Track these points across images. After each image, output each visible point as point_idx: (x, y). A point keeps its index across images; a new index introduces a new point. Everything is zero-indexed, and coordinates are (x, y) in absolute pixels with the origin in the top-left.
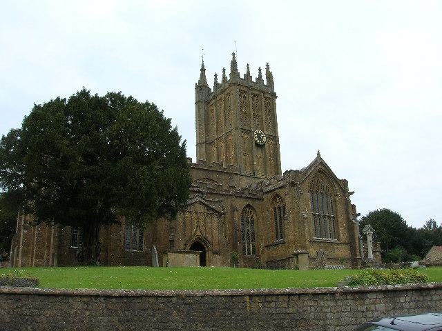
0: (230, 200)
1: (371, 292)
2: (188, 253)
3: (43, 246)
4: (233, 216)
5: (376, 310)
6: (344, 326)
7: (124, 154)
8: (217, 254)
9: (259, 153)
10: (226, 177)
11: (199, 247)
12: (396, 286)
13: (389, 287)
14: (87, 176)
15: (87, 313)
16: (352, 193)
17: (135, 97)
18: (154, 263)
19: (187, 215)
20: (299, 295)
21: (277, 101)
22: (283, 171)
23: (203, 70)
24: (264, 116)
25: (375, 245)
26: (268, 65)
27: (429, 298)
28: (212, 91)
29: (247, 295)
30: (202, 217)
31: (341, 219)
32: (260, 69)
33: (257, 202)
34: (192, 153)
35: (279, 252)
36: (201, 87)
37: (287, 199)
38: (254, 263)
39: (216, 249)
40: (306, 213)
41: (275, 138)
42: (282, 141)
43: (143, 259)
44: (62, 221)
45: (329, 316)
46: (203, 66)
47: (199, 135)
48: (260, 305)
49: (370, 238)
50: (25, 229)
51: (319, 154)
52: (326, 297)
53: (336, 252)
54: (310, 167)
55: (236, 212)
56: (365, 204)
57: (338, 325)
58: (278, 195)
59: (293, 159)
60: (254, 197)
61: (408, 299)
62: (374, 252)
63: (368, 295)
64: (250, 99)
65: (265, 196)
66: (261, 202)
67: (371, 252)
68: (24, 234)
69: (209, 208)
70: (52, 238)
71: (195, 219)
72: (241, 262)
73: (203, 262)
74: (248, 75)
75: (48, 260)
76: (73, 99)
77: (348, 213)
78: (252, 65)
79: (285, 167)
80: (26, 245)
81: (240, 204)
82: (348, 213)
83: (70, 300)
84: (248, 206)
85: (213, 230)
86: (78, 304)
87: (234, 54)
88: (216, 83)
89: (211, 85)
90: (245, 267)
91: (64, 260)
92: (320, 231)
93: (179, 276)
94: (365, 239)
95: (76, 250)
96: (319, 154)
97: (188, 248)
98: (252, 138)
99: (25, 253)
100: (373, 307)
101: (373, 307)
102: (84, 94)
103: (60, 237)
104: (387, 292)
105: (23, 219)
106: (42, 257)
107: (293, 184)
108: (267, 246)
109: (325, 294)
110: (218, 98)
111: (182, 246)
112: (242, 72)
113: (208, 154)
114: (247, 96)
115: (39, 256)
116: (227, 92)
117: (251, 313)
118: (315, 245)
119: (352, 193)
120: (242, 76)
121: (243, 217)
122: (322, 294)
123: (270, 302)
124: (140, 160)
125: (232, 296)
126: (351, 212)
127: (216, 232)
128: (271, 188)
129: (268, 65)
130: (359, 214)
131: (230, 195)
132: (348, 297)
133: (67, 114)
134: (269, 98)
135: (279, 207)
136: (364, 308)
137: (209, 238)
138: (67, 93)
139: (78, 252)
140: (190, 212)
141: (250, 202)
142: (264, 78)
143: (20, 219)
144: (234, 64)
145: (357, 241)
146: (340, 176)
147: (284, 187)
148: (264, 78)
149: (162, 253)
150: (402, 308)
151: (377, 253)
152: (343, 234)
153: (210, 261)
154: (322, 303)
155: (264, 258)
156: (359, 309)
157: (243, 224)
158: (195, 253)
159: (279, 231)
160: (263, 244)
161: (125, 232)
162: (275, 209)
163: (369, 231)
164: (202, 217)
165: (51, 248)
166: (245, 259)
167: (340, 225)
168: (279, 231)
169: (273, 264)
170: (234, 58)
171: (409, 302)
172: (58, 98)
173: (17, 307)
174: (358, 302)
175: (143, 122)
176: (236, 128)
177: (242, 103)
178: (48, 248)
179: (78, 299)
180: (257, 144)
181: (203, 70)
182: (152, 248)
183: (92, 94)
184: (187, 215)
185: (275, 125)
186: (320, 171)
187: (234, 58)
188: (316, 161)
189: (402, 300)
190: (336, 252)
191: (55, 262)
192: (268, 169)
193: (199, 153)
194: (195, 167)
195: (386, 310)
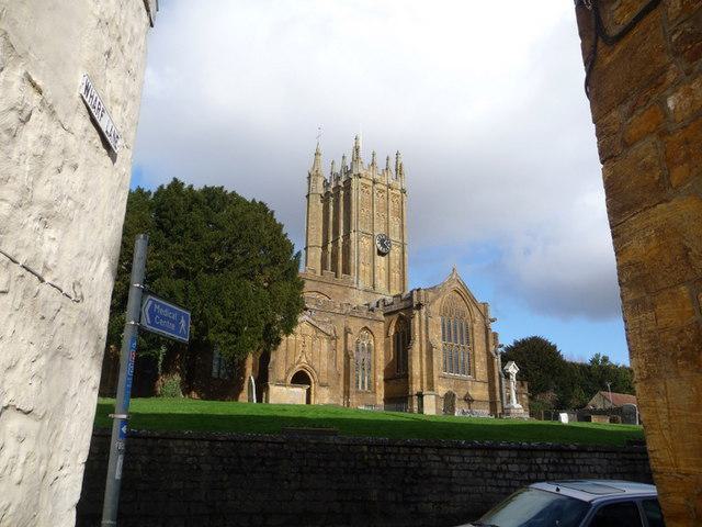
4: (346, 341)
7: (31, 203)
30: (309, 339)
36: (130, 192)
39: (324, 380)
45: (454, 473)
49: (513, 378)
61: (546, 461)
63: (500, 453)
97: (289, 382)
100: (504, 467)
101: (504, 467)
121: (357, 342)
127: (325, 360)
136: (494, 468)
150: (539, 471)
151: (524, 396)
157: (357, 350)
167: (477, 358)
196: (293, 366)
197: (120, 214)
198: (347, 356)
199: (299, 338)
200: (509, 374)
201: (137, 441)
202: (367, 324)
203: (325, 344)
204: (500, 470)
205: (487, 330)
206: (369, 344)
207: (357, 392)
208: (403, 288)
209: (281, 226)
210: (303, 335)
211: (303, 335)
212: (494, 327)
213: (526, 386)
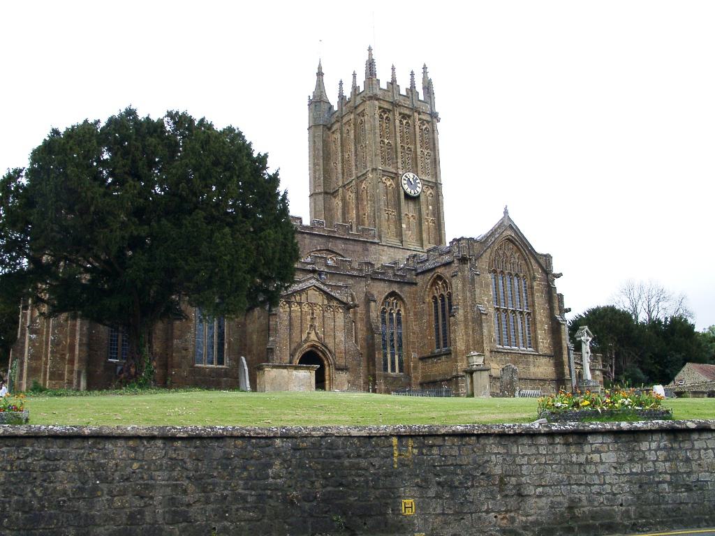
0: (363, 284)
1: (595, 432)
2: (296, 368)
3: (63, 357)
4: (368, 311)
5: (602, 463)
6: (550, 486)
8: (342, 370)
9: (408, 210)
10: (359, 248)
11: (312, 358)
12: (635, 424)
13: (624, 425)
14: (136, 243)
15: (135, 466)
16: (559, 276)
17: (209, 120)
18: (242, 387)
19: (295, 308)
20: (478, 436)
21: (439, 126)
22: (449, 237)
23: (320, 74)
24: (419, 150)
25: (594, 358)
26: (425, 68)
27: (687, 445)
28: (336, 108)
29: (393, 436)
30: (318, 311)
31: (541, 315)
32: (412, 74)
33: (406, 288)
34: (300, 206)
35: (439, 368)
36: (317, 102)
37: (457, 284)
38: (401, 386)
39: (341, 362)
40: (487, 304)
41: (436, 186)
42: (446, 191)
43: (226, 380)
44: (95, 318)
45: (525, 470)
46: (320, 68)
47: (314, 180)
48: (415, 451)
49: (586, 348)
50: (32, 332)
51: (506, 212)
52: (521, 440)
53: (532, 369)
54: (492, 233)
55: (373, 304)
56: (580, 295)
57: (540, 486)
58: (439, 278)
59: (466, 218)
60: (402, 279)
61: (654, 445)
62: (592, 370)
63: (589, 438)
64: (397, 122)
65: (419, 280)
66: (414, 288)
67: (587, 366)
68: (30, 339)
69: (330, 297)
70: (77, 347)
71: (306, 312)
72: (381, 383)
73: (320, 383)
74: (393, 83)
75: (70, 383)
76: (112, 121)
77: (551, 309)
78: (399, 68)
79: (454, 229)
80: (34, 357)
81: (380, 290)
82: (551, 309)
83: (109, 446)
84: (393, 294)
85: (336, 333)
86: (119, 451)
87: (370, 49)
88: (341, 97)
89: (334, 100)
90: (388, 392)
91: (102, 379)
92: (507, 335)
93: (286, 402)
94: (578, 347)
95: (116, 365)
96: (506, 212)
97: (296, 361)
98: (398, 185)
99: (33, 371)
100: (596, 457)
101: (596, 457)
102: (130, 112)
103: (91, 344)
104: (618, 433)
105: (29, 316)
106: (61, 377)
107: (463, 260)
108: (422, 359)
109: (520, 435)
110: (345, 120)
111: (287, 359)
112: (384, 78)
113: (328, 210)
114: (391, 116)
115: (56, 375)
116: (360, 110)
117: (402, 464)
118: (499, 357)
119: (559, 276)
120: (383, 85)
121: (383, 312)
122: (515, 435)
123: (432, 446)
124: (217, 218)
125: (370, 437)
126: (556, 305)
127: (341, 336)
128: (428, 265)
129: (425, 68)
130: (569, 310)
131: (362, 277)
132: (557, 440)
133: (100, 144)
134: (428, 122)
135: (442, 296)
136: (582, 459)
137: (331, 346)
138: (101, 112)
139: (119, 368)
140: (300, 304)
141: (395, 288)
142: (419, 88)
143: (25, 316)
144: (371, 65)
145: (565, 352)
146: (540, 249)
147: (448, 264)
148: (419, 88)
149: (256, 370)
151: (597, 373)
152: (544, 343)
153: (331, 381)
154: (514, 450)
155: (417, 376)
156: (574, 459)
158: (308, 368)
159: (441, 336)
160: (414, 355)
161: (198, 331)
162: (434, 297)
163: (586, 338)
164: (318, 311)
165: (76, 361)
166: (386, 377)
167: (539, 326)
168: (441, 336)
169: (432, 386)
170: (370, 55)
171: (656, 451)
172: (86, 121)
173: (18, 458)
174: (573, 449)
175: (219, 160)
176: (374, 170)
177: (380, 129)
178: (71, 362)
179: (121, 443)
180: (407, 196)
181: (320, 74)
182: (238, 361)
183: (141, 116)
184: (295, 308)
185: (435, 162)
186: (510, 240)
187: (370, 55)
188: (500, 225)
189: (644, 446)
190: (532, 369)
191: (83, 383)
192: (425, 236)
193: (314, 211)
194: (309, 232)
195: (617, 463)
196: (300, 345)
197: (56, 401)
198: (371, 330)
199: (306, 308)
200: (580, 342)
201: (361, 174)
202: (395, 288)
203: (340, 316)
204: (589, 462)
205: (550, 290)
206: (398, 314)
207: (386, 377)
208: (440, 240)
209: (263, 160)
210: (312, 305)
211: (312, 305)
212: (560, 286)
213: (600, 359)
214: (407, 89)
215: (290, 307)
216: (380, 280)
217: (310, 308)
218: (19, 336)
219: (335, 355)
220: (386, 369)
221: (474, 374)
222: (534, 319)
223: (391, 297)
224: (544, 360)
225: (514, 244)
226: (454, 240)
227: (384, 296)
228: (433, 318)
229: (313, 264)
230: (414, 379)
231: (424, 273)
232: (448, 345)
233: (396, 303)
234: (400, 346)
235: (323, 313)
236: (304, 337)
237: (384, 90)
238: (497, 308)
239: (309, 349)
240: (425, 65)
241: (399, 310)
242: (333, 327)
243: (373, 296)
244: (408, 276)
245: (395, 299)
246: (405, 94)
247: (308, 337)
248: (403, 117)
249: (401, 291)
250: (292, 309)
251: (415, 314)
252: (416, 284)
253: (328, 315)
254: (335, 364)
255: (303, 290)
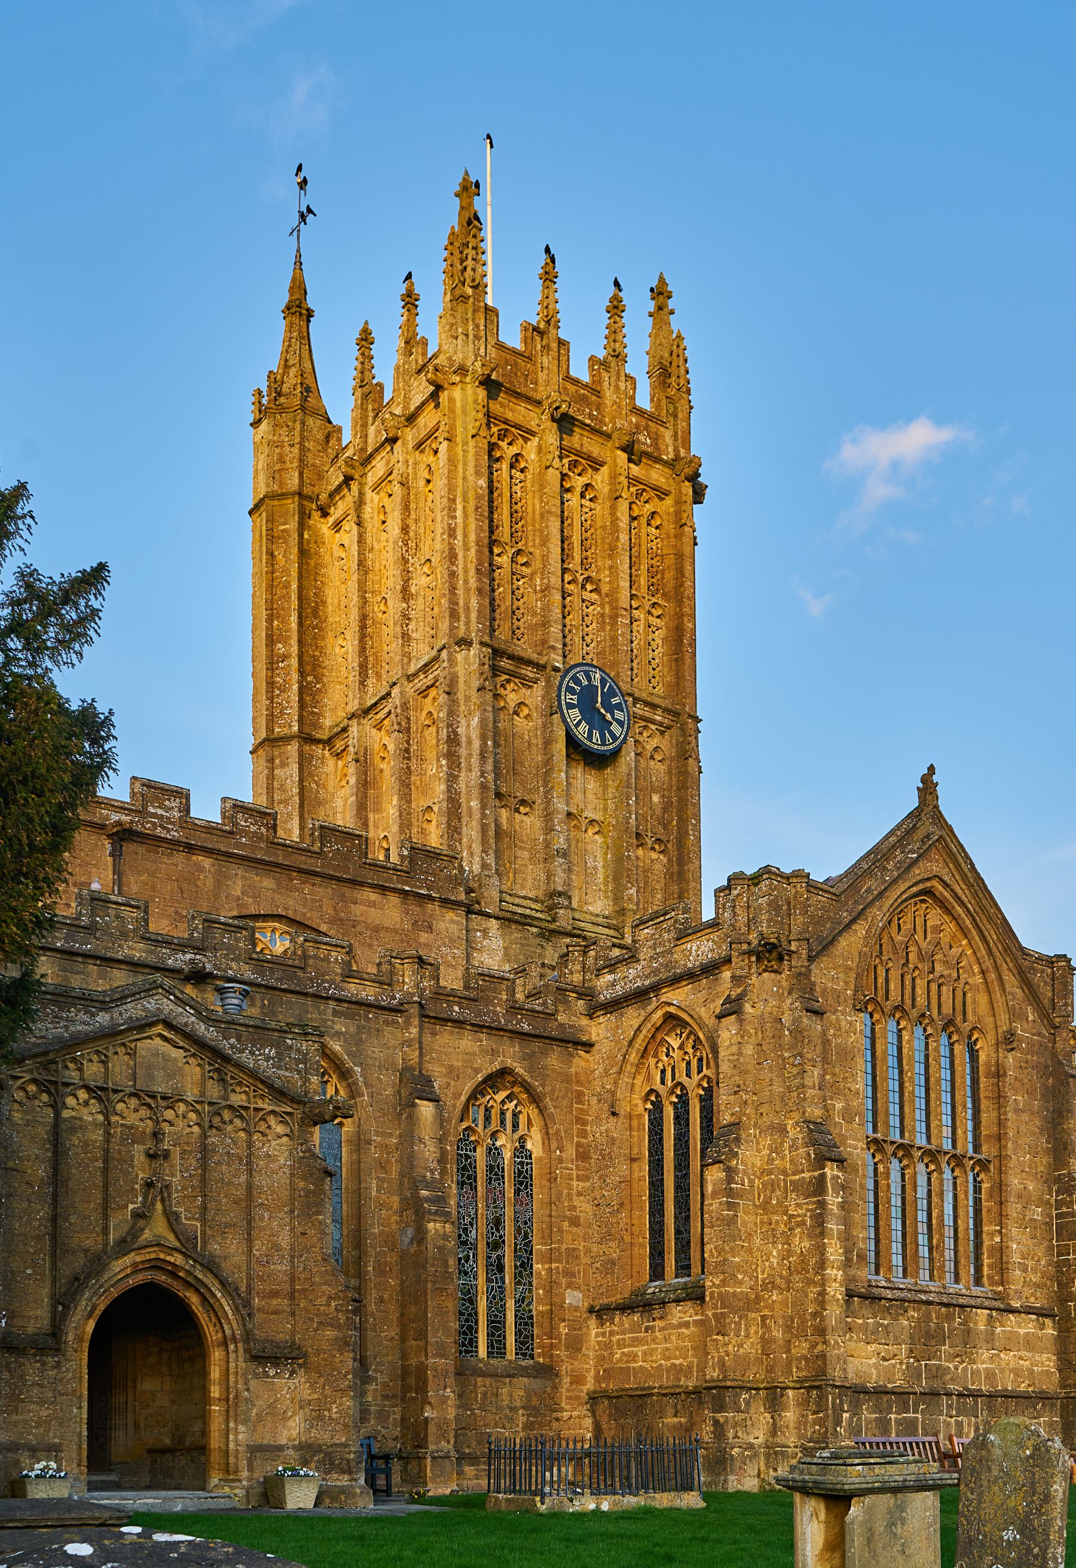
8: (275, 1360)
51: (928, 788)
55: (426, 1109)
65: (598, 1030)
96: (928, 788)
140: (100, 1093)
141: (511, 1056)
167: (1013, 1209)
196: (98, 1263)
206: (521, 1150)
214: (592, 359)
215: (57, 1106)
216: (459, 1023)
217: (144, 1112)
218: (374, 1194)
219: (247, 1304)
220: (468, 1343)
221: (855, 1510)
222: (1000, 1188)
223: (496, 1089)
224: (1025, 1327)
225: (948, 911)
226: (735, 879)
227: (469, 1087)
228: (643, 1169)
229: (199, 949)
230: (567, 1380)
231: (614, 1006)
232: (696, 1269)
233: (515, 1115)
234: (524, 1266)
235: (204, 1135)
236: (119, 1223)
237: (514, 352)
238: (875, 1141)
239: (140, 1278)
240: (662, 280)
241: (522, 1140)
242: (240, 1193)
243: (429, 1082)
244: (561, 1018)
245: (510, 1098)
246: (585, 377)
247: (134, 1233)
248: (573, 465)
249: (530, 1071)
250: (66, 1114)
251: (583, 1156)
252: (588, 1046)
253: (231, 1138)
254: (248, 1337)
255: (111, 1034)
